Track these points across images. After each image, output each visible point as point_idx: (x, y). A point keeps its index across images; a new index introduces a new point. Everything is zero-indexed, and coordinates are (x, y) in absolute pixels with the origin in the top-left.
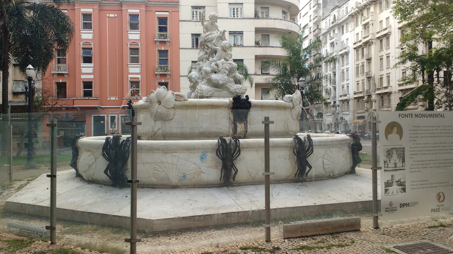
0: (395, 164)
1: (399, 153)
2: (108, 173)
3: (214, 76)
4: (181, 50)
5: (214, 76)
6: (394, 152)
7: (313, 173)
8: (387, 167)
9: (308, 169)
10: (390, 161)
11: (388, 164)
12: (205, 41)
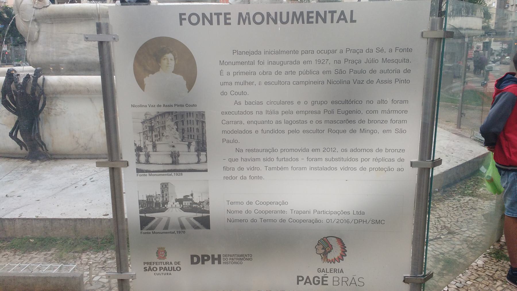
6: (169, 122)
8: (147, 162)
10: (154, 146)
11: (148, 156)
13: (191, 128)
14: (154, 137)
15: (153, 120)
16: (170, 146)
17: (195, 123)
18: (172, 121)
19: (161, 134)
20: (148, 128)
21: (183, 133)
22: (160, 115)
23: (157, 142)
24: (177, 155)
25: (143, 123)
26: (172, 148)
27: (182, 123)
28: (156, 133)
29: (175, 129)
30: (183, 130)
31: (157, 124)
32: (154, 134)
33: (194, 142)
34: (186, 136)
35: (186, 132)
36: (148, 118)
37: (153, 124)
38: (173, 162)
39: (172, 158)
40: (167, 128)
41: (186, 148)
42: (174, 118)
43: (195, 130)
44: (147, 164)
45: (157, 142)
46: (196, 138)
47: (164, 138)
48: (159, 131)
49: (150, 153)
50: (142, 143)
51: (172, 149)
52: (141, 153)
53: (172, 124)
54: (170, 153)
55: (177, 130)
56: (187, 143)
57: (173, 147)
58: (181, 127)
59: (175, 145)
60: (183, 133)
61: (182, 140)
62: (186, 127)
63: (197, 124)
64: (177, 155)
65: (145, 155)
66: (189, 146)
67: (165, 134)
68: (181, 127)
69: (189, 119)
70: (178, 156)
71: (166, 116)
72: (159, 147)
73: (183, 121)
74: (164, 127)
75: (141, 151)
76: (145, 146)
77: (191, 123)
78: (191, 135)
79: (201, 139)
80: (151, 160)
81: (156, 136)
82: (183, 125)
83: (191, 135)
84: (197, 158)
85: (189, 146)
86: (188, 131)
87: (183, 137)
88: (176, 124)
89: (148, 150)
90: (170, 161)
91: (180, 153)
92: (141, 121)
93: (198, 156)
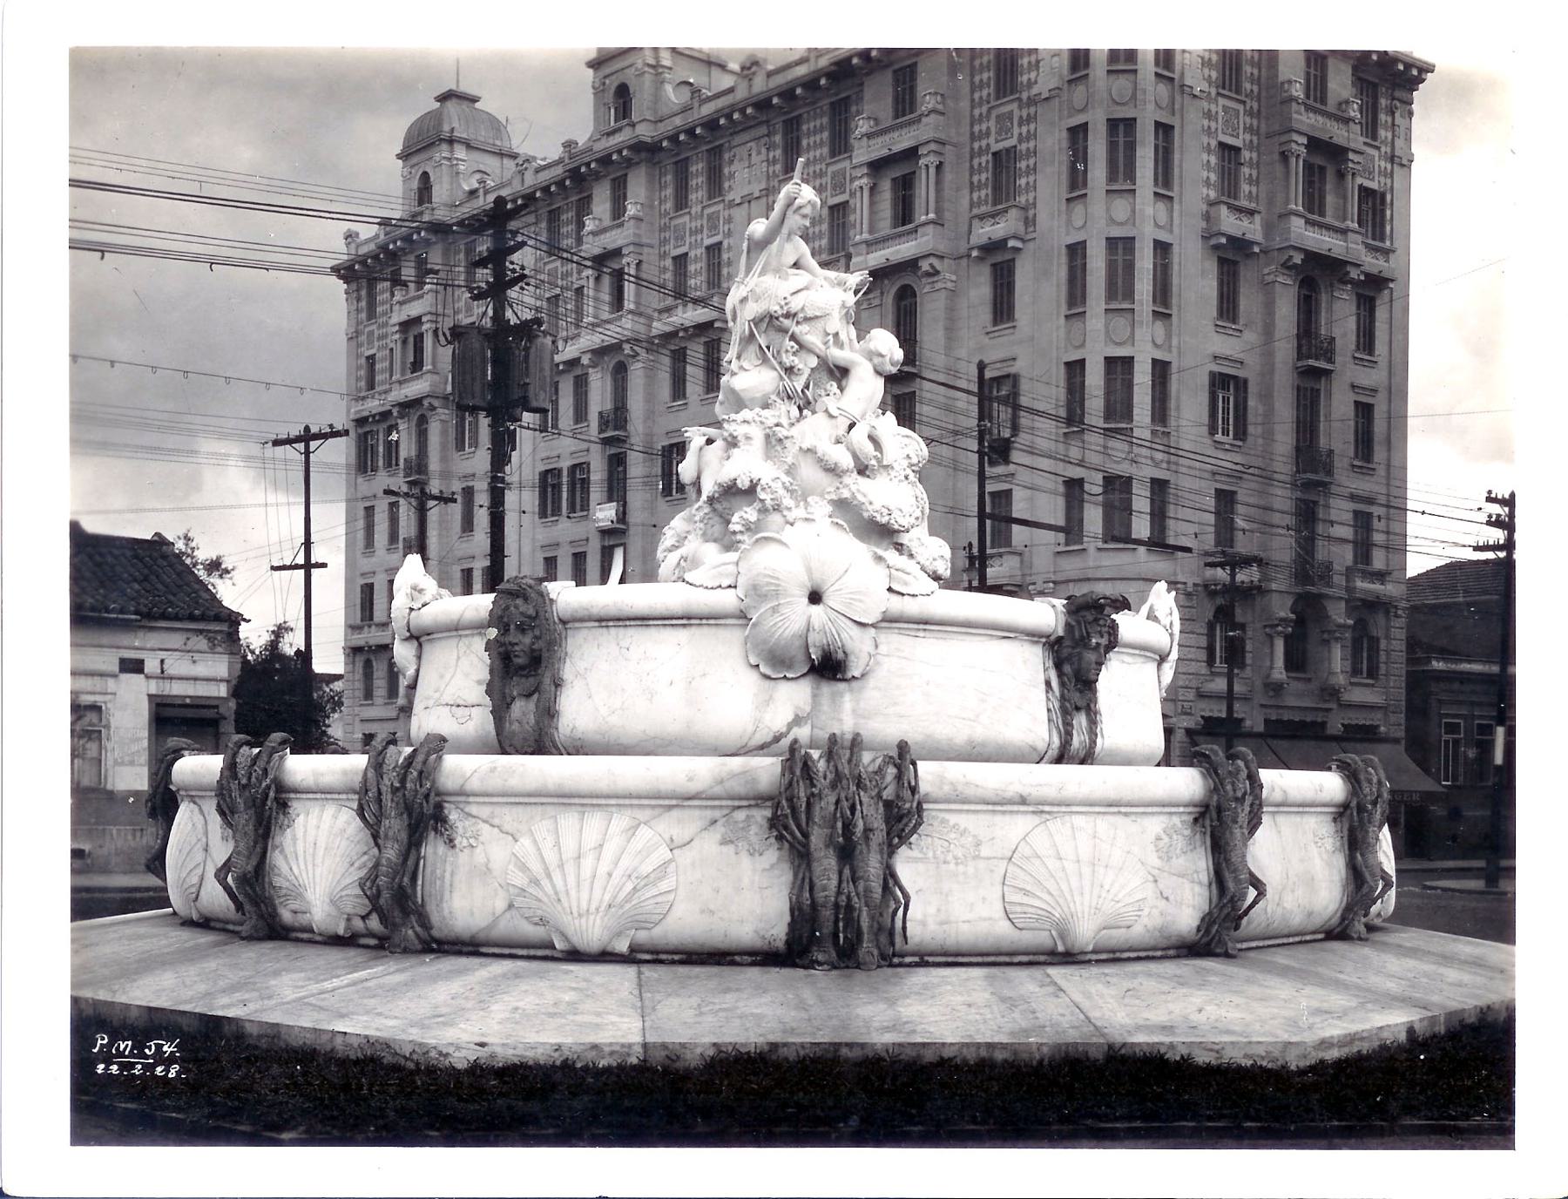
0: (838, 822)
1: (1037, 347)
2: (230, 879)
3: (856, 486)
4: (1061, 522)
5: (856, 486)
6: (792, 282)
7: (1257, 919)
8: (396, 919)
9: (1252, 893)
10: (525, 662)
11: (411, 811)
12: (788, 316)
13: (1119, 367)
14: (520, 501)
15: (529, 228)
16: (776, 662)
17: (1197, 281)
18: (835, 254)
19: (637, 467)
20: (440, 356)
21: (996, 451)
22: (646, 151)
23: (565, 594)
24: (871, 814)
25: (366, 274)
26: (794, 696)
27: (980, 289)
28: (565, 449)
29: (866, 388)
30: (996, 391)
31: (596, 302)
32: (531, 452)
33: (1162, 599)
34: (1035, 499)
35: (1041, 434)
36: (447, 200)
37: (523, 304)
38: (804, 917)
39: (800, 855)
40: (747, 376)
41: (1188, 75)
42: (870, 210)
43: (1190, 407)
44: (384, 945)
45: (565, 594)
46: (1192, 524)
47: (682, 533)
48: (617, 417)
49: (457, 768)
50: (331, 592)
51: (787, 705)
52: (300, 767)
53: (828, 294)
54: (767, 769)
55: (901, 397)
56: (1046, 614)
57: (829, 667)
58: (961, 337)
59: (858, 644)
60: (996, 451)
61: (974, 572)
62: (1037, 347)
63: (1228, 308)
64: (871, 814)
65: (369, 802)
66: (1075, 660)
67: (707, 465)
68: (961, 337)
69: (1099, 219)
70: (904, 819)
71: (744, 174)
72: (601, 684)
73: (1000, 262)
74: (697, 355)
75: (312, 741)
76: (369, 656)
77: (1120, 285)
78: (1118, 486)
79: (1283, 548)
80: (472, 881)
81: (560, 491)
82: (1003, 309)
83: (1118, 486)
84: (1200, 863)
85: (1075, 660)
86: (1074, 416)
87: (996, 516)
88: (896, 297)
89: (427, 720)
90: (747, 893)
91: (928, 773)
92: (329, 239)
93: (1221, 824)
